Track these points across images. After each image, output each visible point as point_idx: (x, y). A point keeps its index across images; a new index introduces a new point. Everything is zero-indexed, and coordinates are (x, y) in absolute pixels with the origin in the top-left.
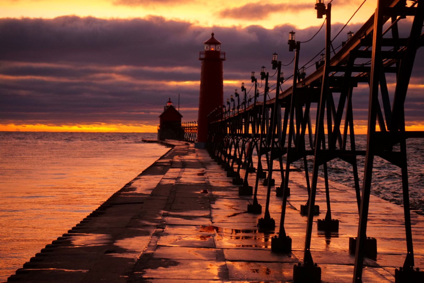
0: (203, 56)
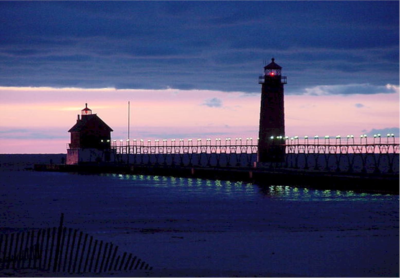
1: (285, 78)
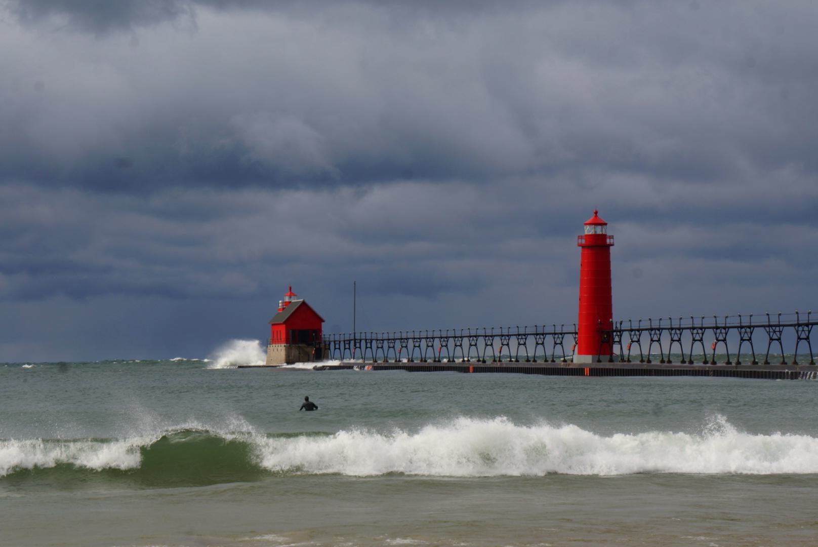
0: (583, 241)
1: (611, 237)
